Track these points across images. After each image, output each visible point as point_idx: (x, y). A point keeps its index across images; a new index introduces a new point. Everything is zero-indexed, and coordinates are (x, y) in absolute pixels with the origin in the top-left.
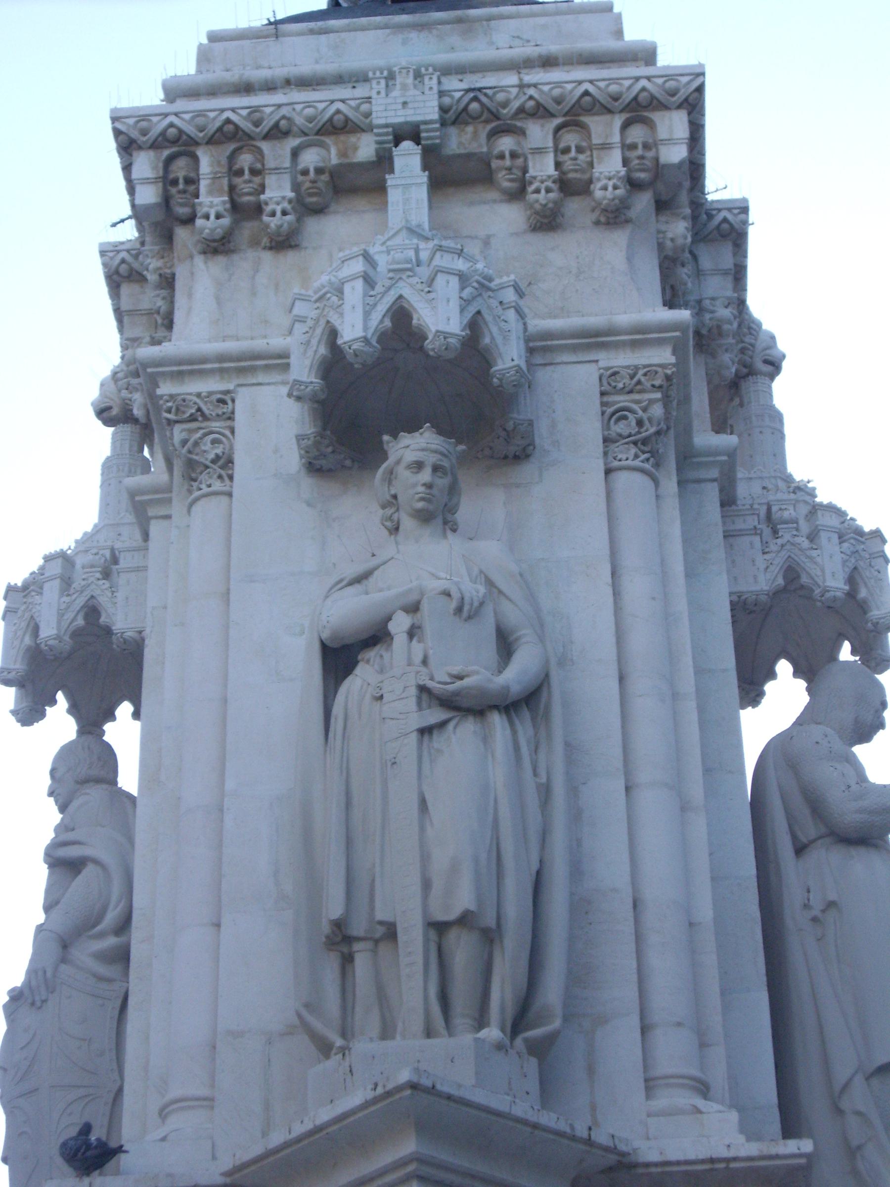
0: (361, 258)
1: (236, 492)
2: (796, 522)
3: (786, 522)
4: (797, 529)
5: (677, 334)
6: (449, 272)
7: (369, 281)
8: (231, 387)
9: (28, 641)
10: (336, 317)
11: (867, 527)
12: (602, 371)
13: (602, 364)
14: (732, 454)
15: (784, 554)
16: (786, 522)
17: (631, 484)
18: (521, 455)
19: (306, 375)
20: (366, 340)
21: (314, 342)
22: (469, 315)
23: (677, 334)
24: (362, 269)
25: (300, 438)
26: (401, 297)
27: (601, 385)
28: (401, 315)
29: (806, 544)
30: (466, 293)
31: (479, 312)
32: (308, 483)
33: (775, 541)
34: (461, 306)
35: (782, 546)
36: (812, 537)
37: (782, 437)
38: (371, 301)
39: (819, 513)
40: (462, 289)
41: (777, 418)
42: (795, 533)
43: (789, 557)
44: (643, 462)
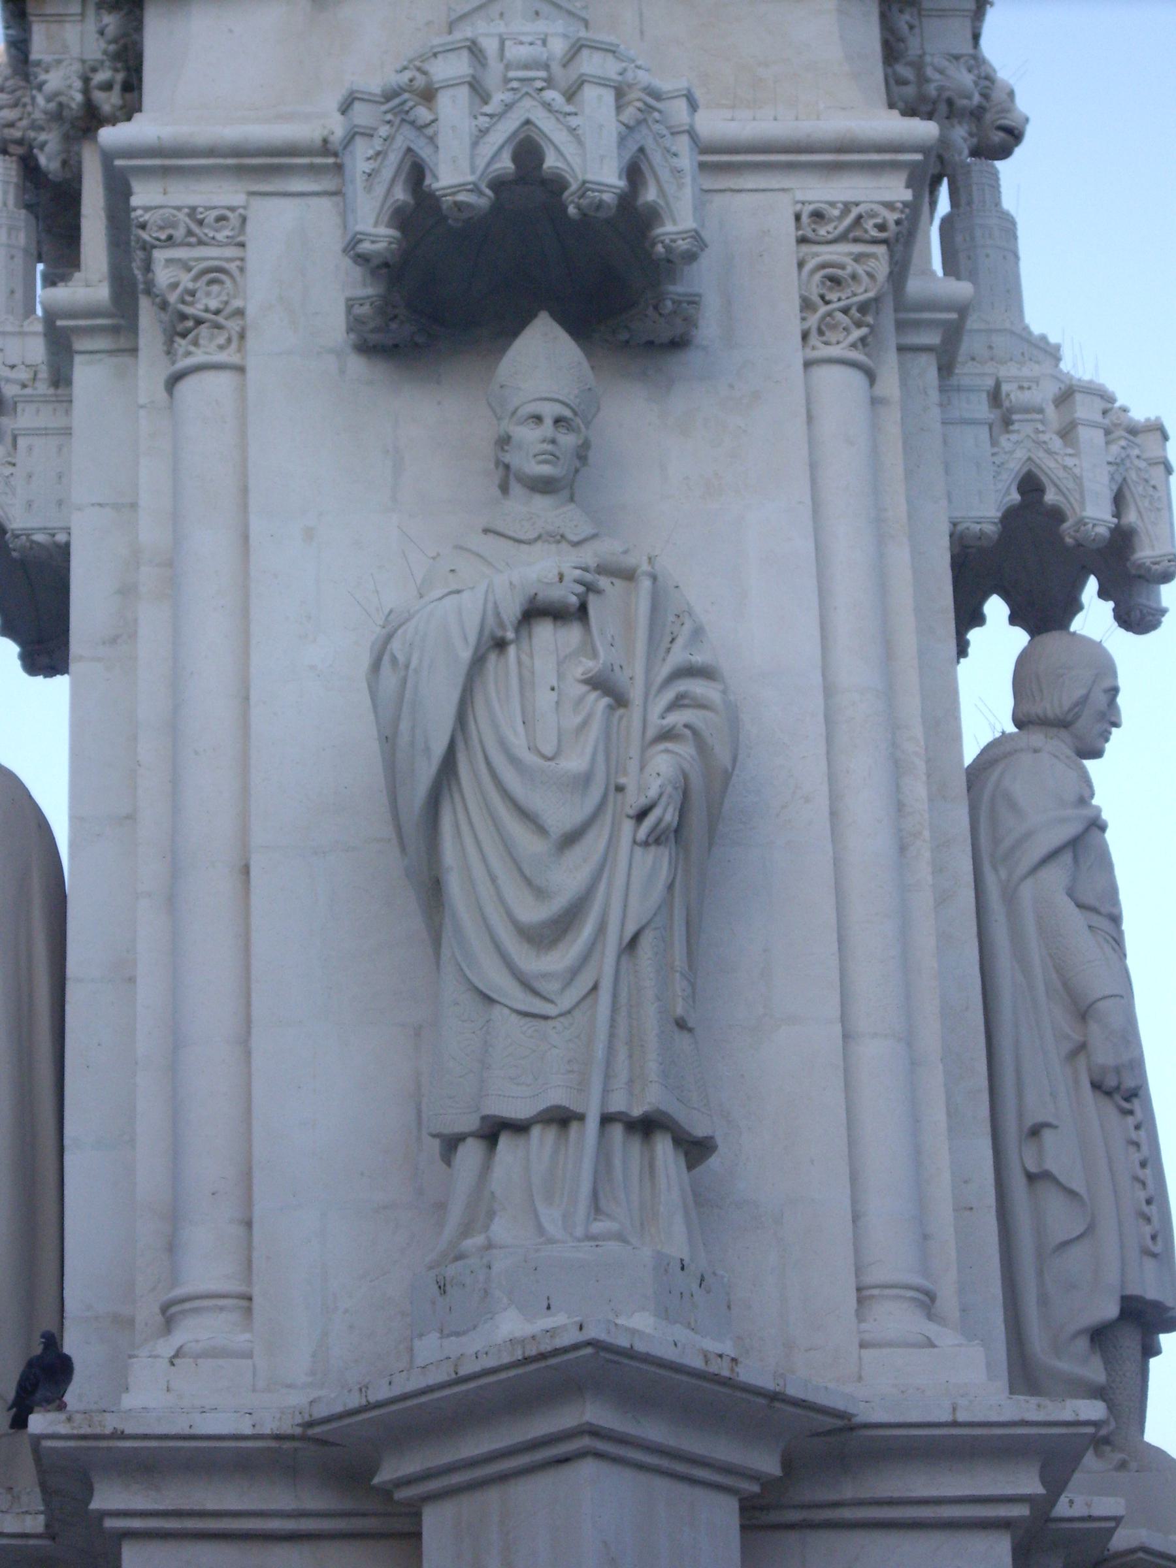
0: (465, 54)
1: (251, 364)
2: (1041, 411)
3: (1027, 410)
4: (1042, 422)
5: (918, 157)
6: (603, 83)
7: (478, 90)
8: (238, 199)
9: (400, 194)
10: (422, 142)
11: (1139, 413)
12: (799, 207)
13: (800, 196)
14: (963, 310)
15: (1021, 454)
16: (1027, 410)
17: (840, 388)
18: (679, 344)
19: (372, 221)
20: (476, 189)
21: (387, 173)
22: (627, 155)
23: (918, 157)
24: (470, 71)
25: (350, 304)
26: (528, 122)
27: (798, 228)
28: (528, 151)
29: (1057, 444)
30: (629, 114)
31: (641, 150)
32: (357, 364)
33: (1007, 436)
34: (620, 133)
35: (1017, 442)
36: (1067, 432)
37: (1017, 257)
38: (483, 121)
39: (1078, 397)
40: (619, 108)
41: (1009, 226)
42: (1041, 427)
43: (1029, 459)
44: (853, 346)
